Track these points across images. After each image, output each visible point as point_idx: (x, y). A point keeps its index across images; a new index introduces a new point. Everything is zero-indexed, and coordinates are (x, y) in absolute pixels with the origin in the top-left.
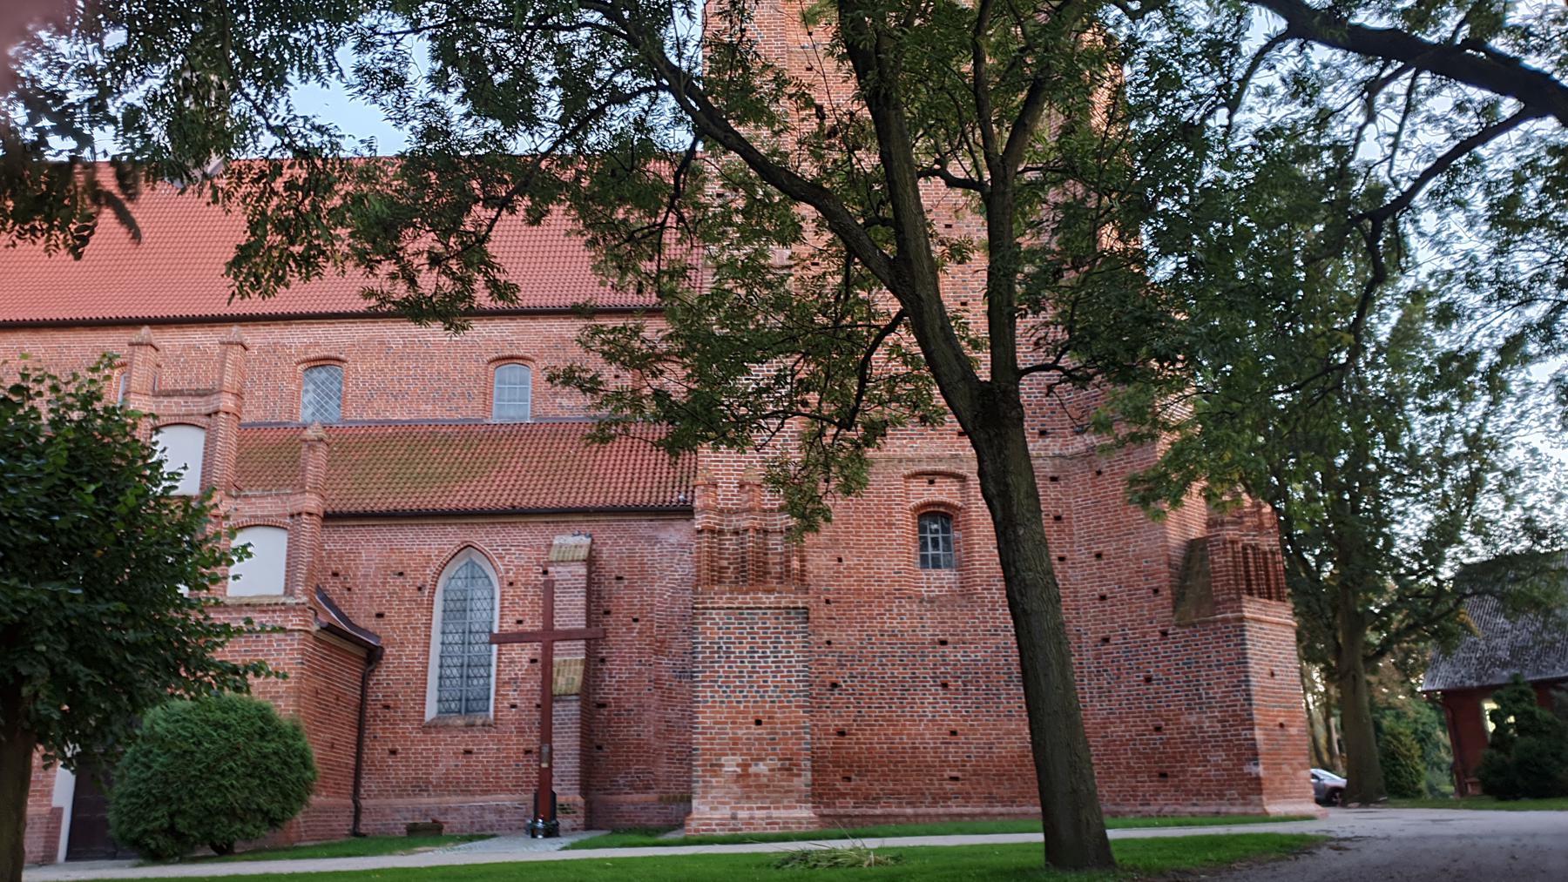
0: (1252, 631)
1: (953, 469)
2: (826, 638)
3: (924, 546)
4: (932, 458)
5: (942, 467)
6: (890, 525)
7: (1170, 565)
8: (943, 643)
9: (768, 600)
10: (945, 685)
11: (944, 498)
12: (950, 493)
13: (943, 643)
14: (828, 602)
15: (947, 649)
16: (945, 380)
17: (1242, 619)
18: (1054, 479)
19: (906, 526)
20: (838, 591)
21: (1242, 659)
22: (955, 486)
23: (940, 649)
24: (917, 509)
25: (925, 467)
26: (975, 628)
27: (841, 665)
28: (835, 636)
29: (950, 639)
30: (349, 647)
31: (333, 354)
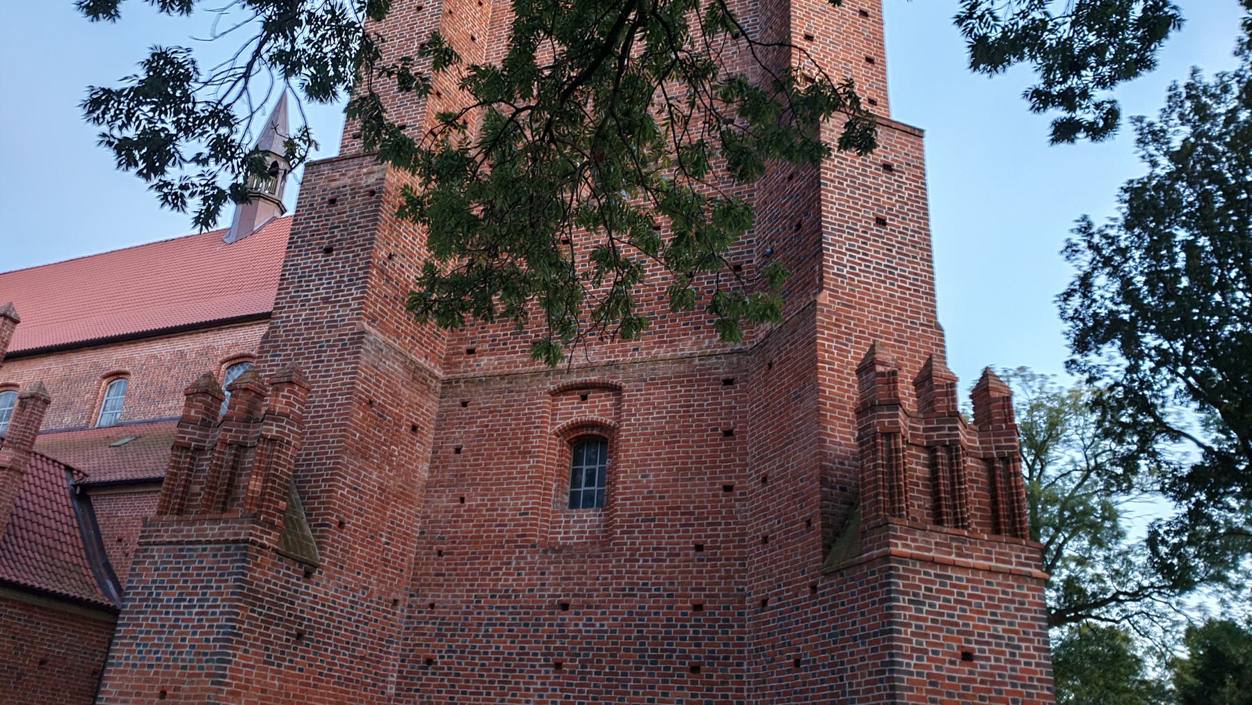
0: (909, 584)
1: (607, 378)
2: (429, 599)
3: (575, 483)
4: (591, 367)
5: (594, 377)
6: (525, 453)
7: (823, 481)
8: (565, 607)
9: (212, 531)
10: (558, 666)
11: (595, 416)
12: (604, 411)
13: (565, 607)
14: (440, 553)
15: (567, 616)
16: (325, 169)
17: (887, 557)
18: (728, 382)
19: (549, 454)
20: (453, 540)
21: (887, 627)
22: (608, 402)
23: (560, 615)
24: (563, 432)
25: (574, 379)
26: (606, 586)
27: (440, 636)
28: (441, 597)
29: (573, 601)
30: (91, 614)
31: (246, 352)
